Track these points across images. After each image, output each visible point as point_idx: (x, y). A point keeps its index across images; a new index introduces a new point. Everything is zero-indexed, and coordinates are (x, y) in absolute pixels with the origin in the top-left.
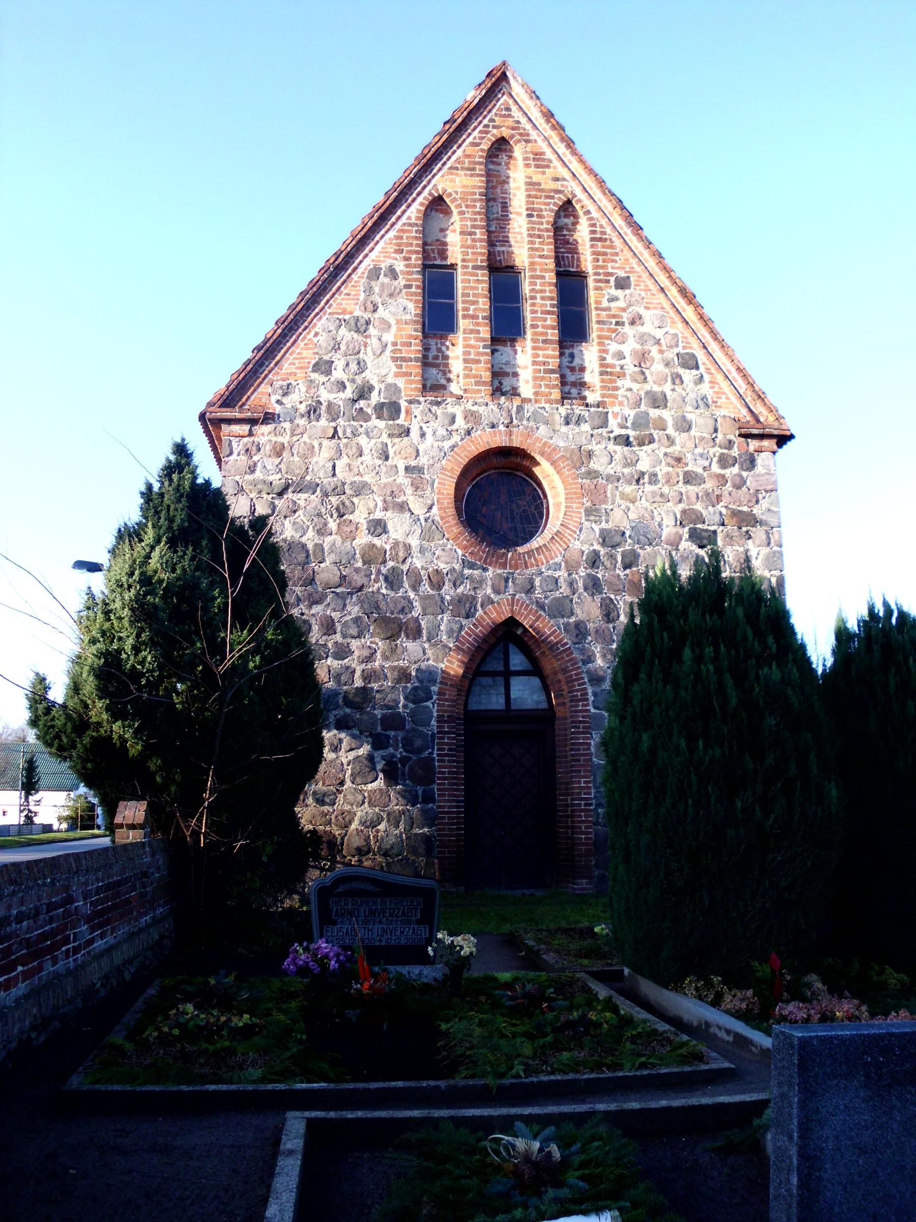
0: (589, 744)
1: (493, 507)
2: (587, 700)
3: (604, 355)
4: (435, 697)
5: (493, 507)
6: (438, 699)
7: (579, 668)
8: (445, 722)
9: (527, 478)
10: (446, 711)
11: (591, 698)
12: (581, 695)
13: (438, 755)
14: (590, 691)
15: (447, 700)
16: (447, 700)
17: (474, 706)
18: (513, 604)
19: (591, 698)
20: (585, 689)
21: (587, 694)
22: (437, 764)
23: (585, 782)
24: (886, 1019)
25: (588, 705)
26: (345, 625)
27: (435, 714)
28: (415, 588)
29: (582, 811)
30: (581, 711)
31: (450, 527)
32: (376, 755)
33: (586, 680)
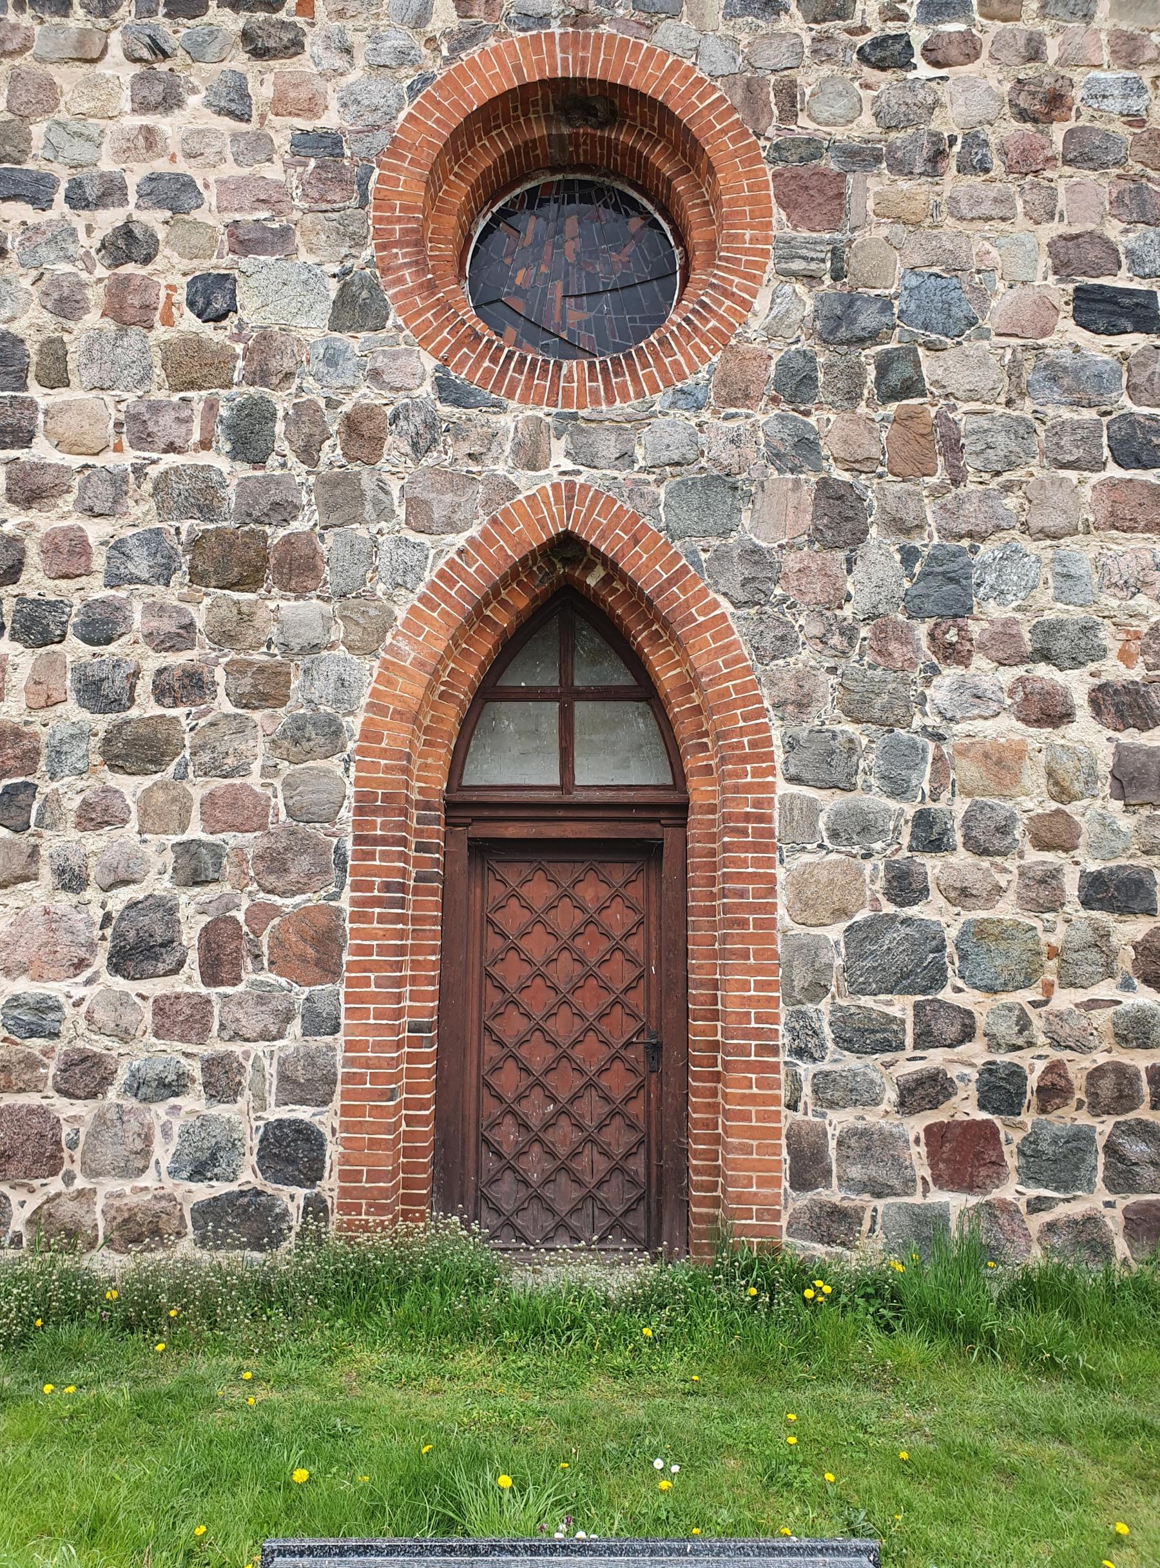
0: (772, 879)
1: (544, 269)
2: (769, 756)
3: (1057, 217)
4: (351, 746)
5: (544, 269)
6: (360, 751)
7: (749, 670)
8: (375, 811)
9: (636, 195)
10: (384, 783)
11: (779, 756)
12: (752, 745)
13: (354, 902)
14: (776, 735)
15: (384, 754)
16: (384, 754)
17: (471, 778)
18: (570, 498)
19: (779, 756)
20: (765, 728)
21: (768, 742)
22: (348, 926)
23: (760, 986)
24: (889, 867)
25: (771, 771)
26: (118, 547)
27: (350, 791)
28: (309, 454)
29: (750, 1067)
30: (748, 788)
31: (405, 294)
32: (183, 899)
33: (767, 704)
